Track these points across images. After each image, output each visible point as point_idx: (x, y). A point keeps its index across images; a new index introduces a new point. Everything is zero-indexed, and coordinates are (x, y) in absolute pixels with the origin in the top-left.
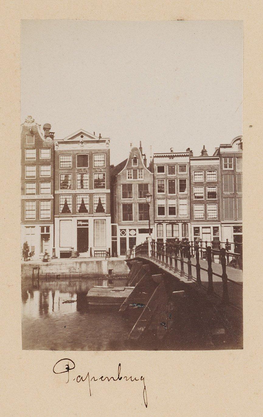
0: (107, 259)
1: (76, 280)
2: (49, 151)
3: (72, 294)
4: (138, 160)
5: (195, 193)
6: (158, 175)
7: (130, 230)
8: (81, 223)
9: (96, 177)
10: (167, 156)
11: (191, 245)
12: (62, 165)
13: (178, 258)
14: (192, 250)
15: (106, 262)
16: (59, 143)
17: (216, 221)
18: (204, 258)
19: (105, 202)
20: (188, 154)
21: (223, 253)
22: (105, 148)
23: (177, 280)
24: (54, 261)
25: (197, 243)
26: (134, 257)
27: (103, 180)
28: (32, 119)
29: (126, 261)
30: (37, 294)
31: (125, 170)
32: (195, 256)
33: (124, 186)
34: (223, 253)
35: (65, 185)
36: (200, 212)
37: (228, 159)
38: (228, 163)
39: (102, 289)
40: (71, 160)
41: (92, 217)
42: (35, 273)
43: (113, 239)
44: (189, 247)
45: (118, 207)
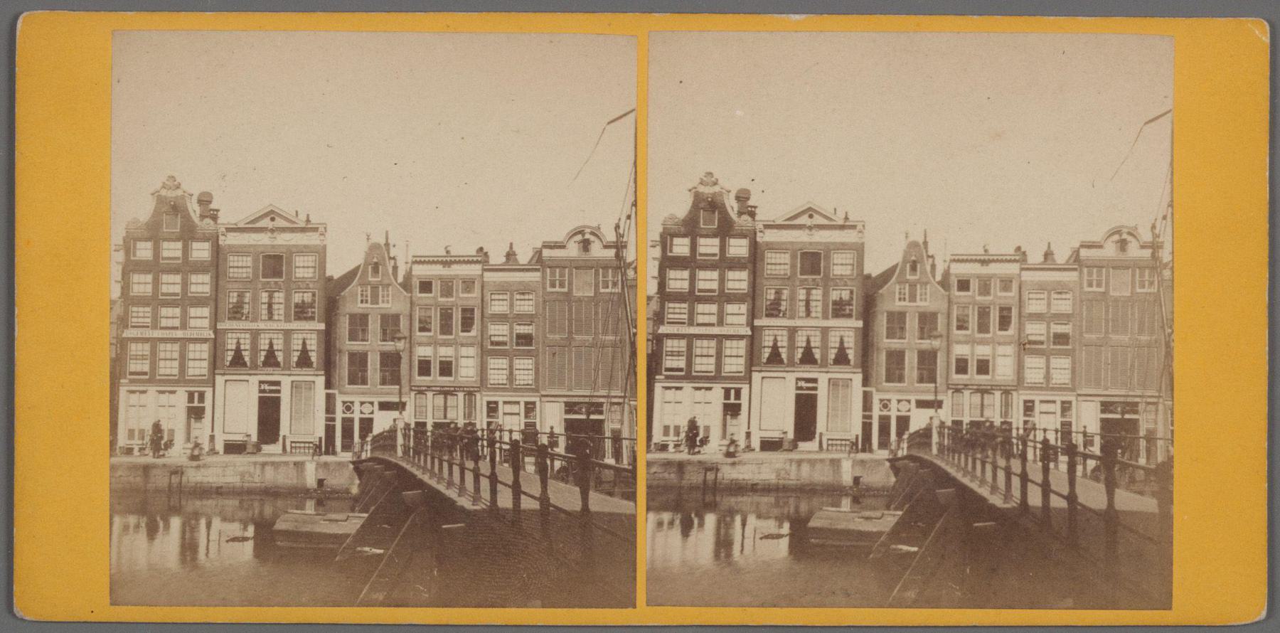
0: (852, 455)
1: (253, 497)
2: (207, 245)
3: (780, 520)
4: (380, 267)
5: (491, 336)
6: (957, 297)
7: (362, 403)
8: (267, 387)
9: (297, 298)
10: (976, 261)
11: (480, 436)
12: (769, 270)
13: (455, 461)
14: (483, 446)
15: (314, 464)
16: (767, 227)
17: (532, 390)
18: (506, 461)
19: (314, 347)
20: (479, 259)
21: (542, 454)
22: (318, 242)
23: (982, 500)
24: (209, 459)
25: (492, 432)
26: (369, 455)
27: (849, 303)
28: (713, 179)
29: (353, 463)
30: (176, 522)
31: (893, 286)
32: (488, 458)
33: (891, 315)
34: (542, 454)
35: (236, 313)
36: (501, 372)
37: (610, 271)
38: (557, 278)
39: (305, 517)
40: (788, 261)
41: (287, 377)
42: (173, 481)
43: (864, 417)
44: (477, 439)
45: (340, 360)
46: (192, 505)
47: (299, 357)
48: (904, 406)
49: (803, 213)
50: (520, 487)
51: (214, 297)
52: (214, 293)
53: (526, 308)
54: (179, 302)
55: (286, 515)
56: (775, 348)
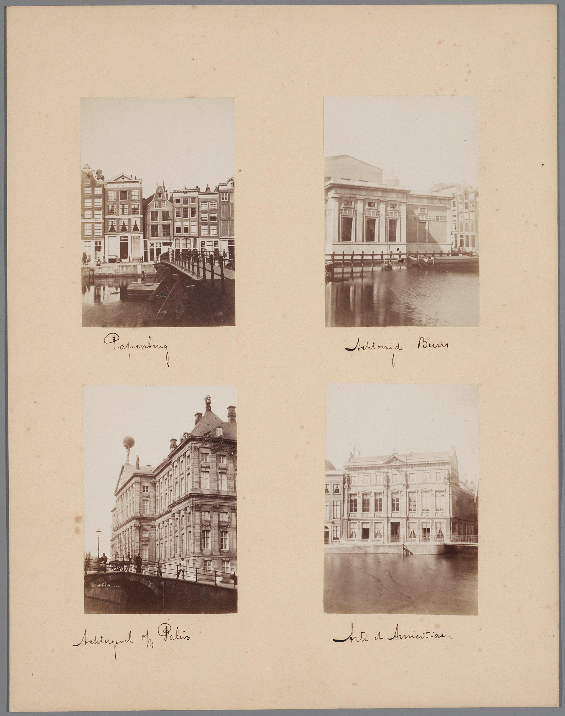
2: (100, 189)
6: (176, 205)
7: (157, 243)
9: (133, 206)
14: (200, 257)
16: (108, 183)
17: (216, 237)
18: (208, 262)
20: (197, 190)
25: (203, 252)
26: (160, 262)
31: (153, 202)
33: (152, 212)
34: (221, 259)
35: (112, 212)
40: (116, 195)
42: (91, 273)
43: (145, 249)
44: (198, 255)
46: (98, 282)
47: (134, 228)
48: (158, 245)
49: (119, 178)
50: (214, 271)
51: (103, 207)
52: (103, 206)
53: (214, 208)
54: (91, 209)
55: (131, 284)
56: (112, 226)
